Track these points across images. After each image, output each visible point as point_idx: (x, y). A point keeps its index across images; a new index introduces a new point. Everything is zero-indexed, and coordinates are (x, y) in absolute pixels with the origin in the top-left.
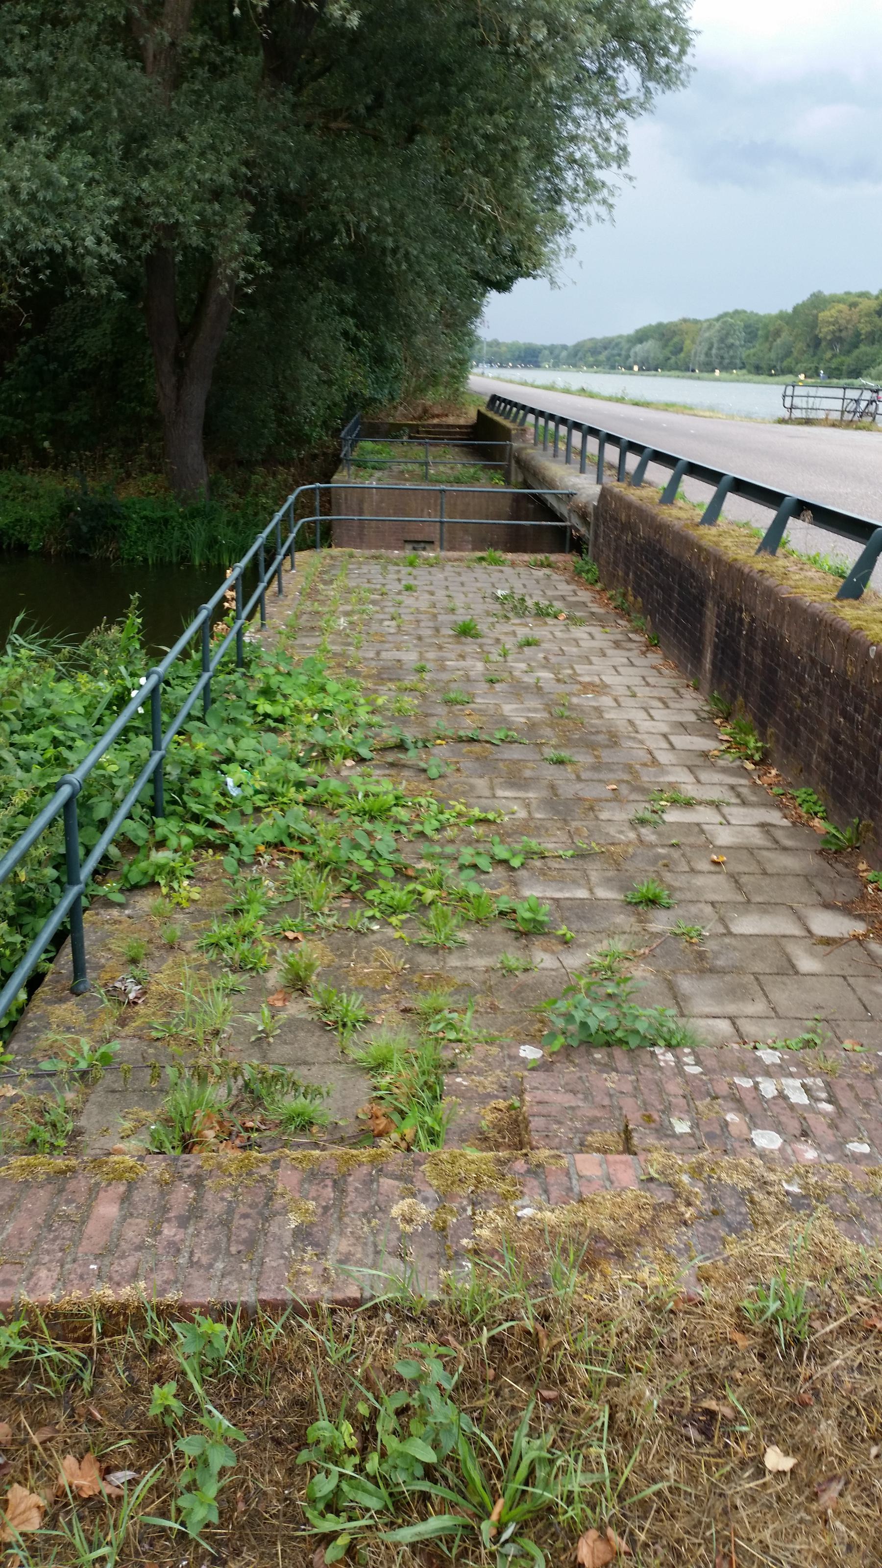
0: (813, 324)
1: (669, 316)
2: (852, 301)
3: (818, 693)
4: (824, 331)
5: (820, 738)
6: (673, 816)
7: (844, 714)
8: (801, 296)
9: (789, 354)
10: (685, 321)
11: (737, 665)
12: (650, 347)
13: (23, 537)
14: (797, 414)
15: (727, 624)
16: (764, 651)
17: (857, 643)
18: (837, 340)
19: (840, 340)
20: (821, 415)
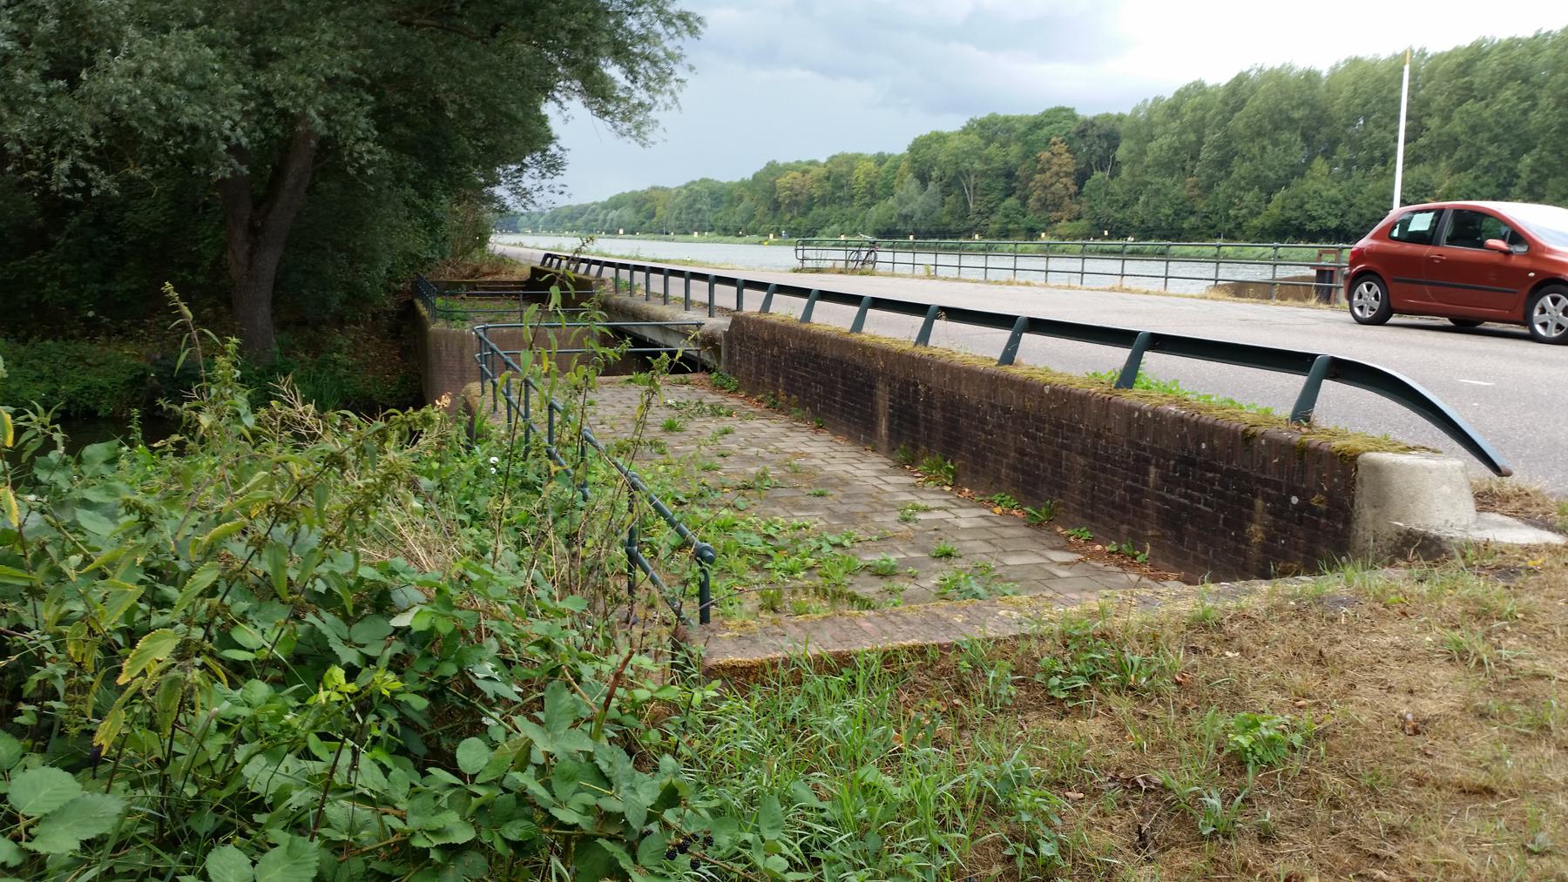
0: (773, 189)
1: (641, 185)
2: (804, 169)
3: (1001, 426)
4: (783, 195)
5: (1006, 456)
6: (922, 516)
7: (1027, 435)
8: (760, 166)
9: (752, 217)
10: (654, 188)
11: (916, 424)
12: (627, 214)
13: (90, 403)
14: (808, 264)
15: (901, 396)
16: (943, 409)
17: (1033, 386)
18: (795, 203)
19: (796, 203)
20: (829, 264)
